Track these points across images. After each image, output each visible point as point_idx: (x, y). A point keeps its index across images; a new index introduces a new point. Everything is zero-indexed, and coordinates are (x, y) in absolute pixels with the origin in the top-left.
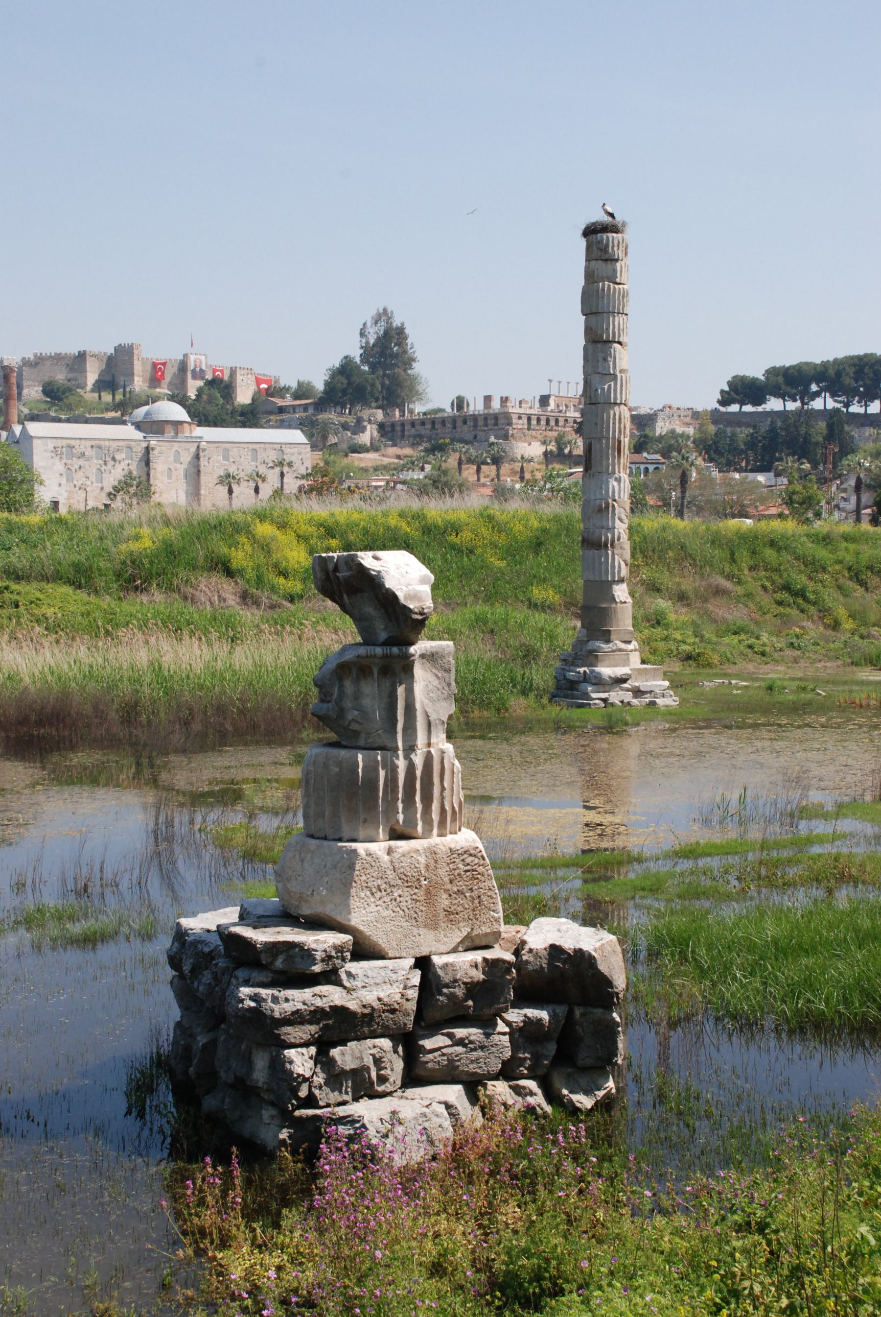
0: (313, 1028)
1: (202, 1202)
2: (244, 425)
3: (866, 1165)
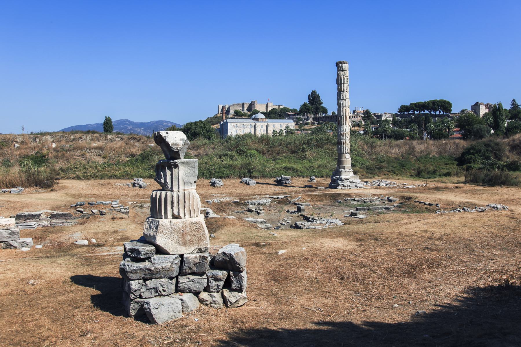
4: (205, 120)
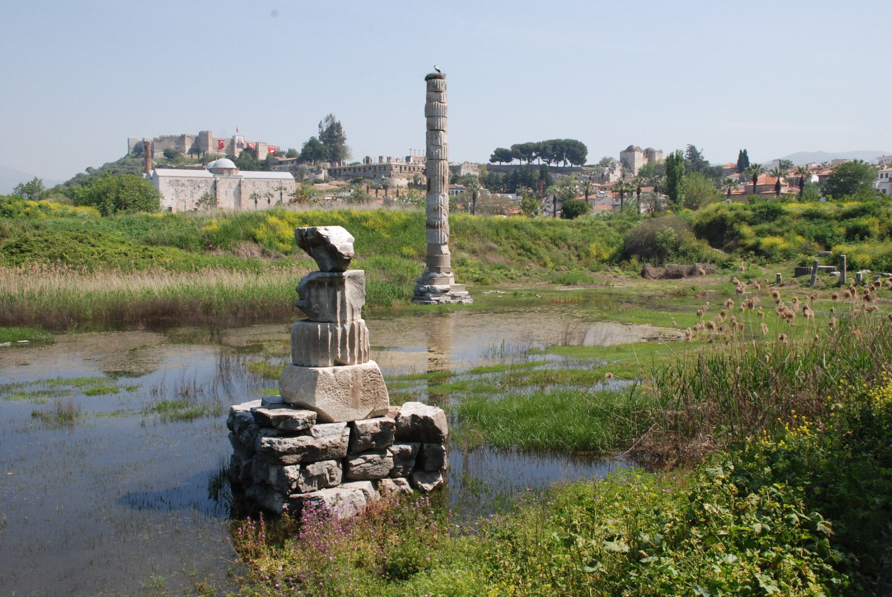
0: (298, 456)
1: (246, 538)
2: (262, 170)
3: (556, 508)
4: (100, 169)
